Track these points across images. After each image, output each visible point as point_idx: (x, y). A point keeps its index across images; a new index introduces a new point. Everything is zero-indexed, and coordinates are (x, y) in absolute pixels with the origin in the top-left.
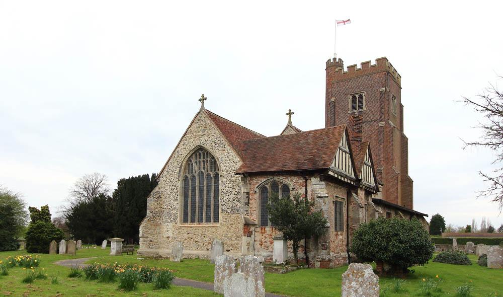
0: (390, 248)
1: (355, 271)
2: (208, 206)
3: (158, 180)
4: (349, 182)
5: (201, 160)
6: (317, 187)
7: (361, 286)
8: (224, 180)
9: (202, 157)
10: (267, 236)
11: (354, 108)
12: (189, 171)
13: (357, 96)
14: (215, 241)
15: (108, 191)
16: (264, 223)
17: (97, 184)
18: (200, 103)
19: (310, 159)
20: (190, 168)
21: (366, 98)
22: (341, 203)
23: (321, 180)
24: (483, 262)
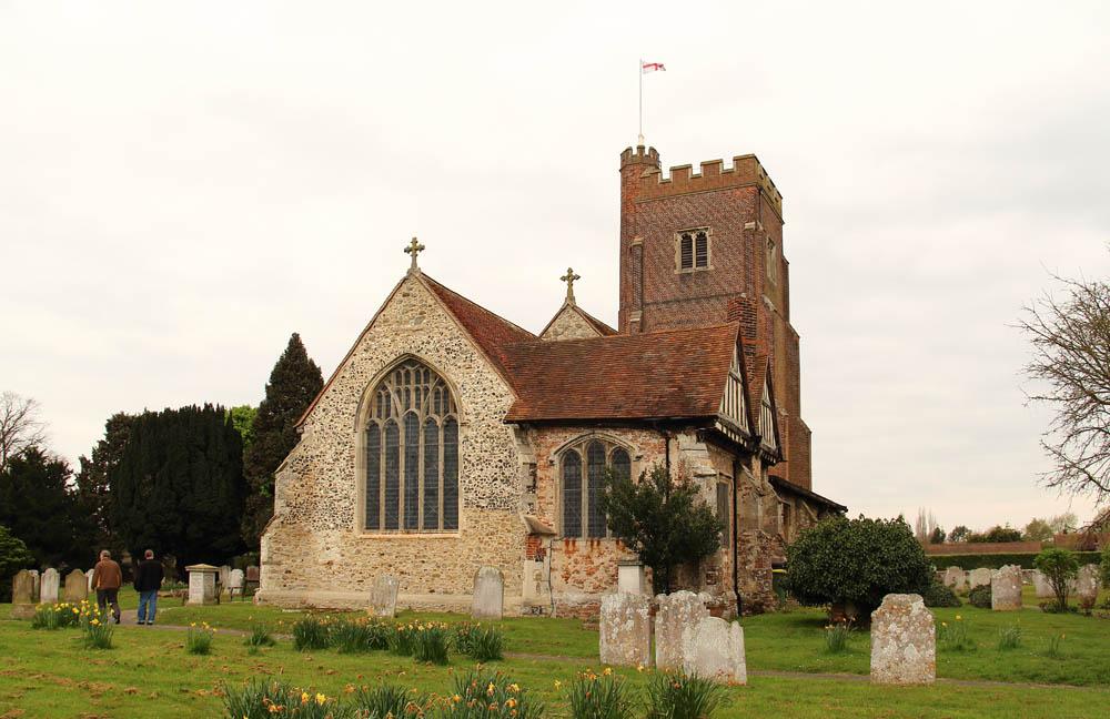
0: (866, 574)
1: (895, 607)
2: (431, 493)
3: (299, 431)
4: (741, 442)
5: (412, 387)
6: (692, 457)
7: (906, 629)
8: (470, 433)
9: (412, 381)
10: (579, 559)
11: (686, 263)
12: (379, 411)
13: (694, 237)
14: (484, 570)
15: (39, 441)
16: (572, 530)
17: (11, 423)
18: (408, 257)
19: (672, 394)
20: (384, 403)
21: (707, 236)
22: (725, 485)
23: (698, 441)
24: (982, 598)
